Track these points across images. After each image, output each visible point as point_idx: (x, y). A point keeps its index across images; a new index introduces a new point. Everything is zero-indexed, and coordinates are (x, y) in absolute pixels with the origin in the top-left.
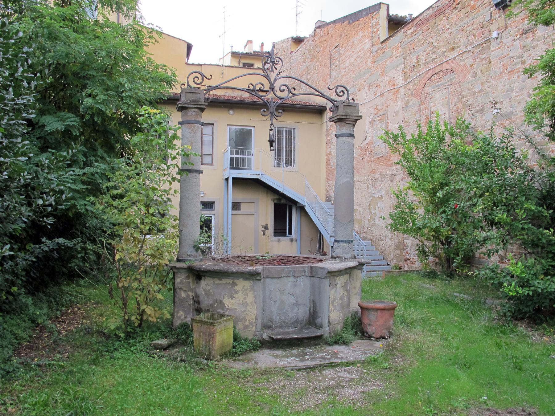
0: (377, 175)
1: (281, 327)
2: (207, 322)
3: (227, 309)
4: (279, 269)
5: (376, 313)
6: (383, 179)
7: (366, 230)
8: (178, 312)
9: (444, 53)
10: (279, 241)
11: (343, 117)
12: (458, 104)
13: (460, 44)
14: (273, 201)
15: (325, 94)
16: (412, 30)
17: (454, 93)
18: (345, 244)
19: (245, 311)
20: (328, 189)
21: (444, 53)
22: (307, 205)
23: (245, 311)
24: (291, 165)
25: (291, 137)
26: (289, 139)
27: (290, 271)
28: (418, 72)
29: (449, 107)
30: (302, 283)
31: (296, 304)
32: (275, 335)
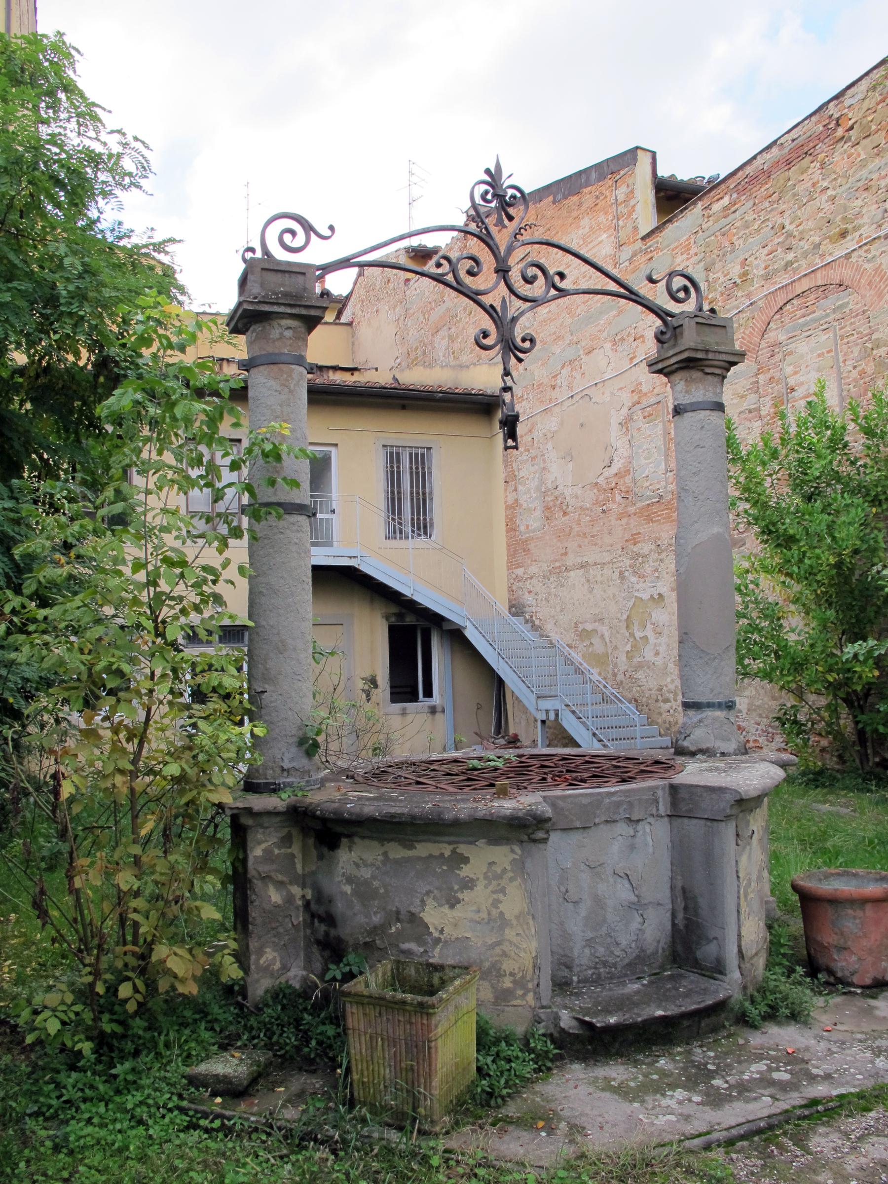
0: (646, 548)
1: (597, 981)
2: (404, 1002)
3: (438, 941)
4: (585, 801)
5: (859, 913)
6: (664, 555)
7: (620, 677)
8: (260, 952)
9: (817, 246)
10: (404, 713)
11: (700, 355)
12: (863, 362)
13: (861, 221)
14: (387, 618)
15: (642, 292)
16: (726, 200)
17: (851, 338)
18: (718, 714)
19: (498, 943)
20: (514, 588)
21: (817, 246)
22: (469, 624)
23: (498, 943)
24: (425, 533)
25: (423, 469)
26: (417, 473)
27: (618, 804)
28: (748, 296)
29: (839, 373)
30: (649, 839)
31: (638, 906)
32: (596, 1014)
